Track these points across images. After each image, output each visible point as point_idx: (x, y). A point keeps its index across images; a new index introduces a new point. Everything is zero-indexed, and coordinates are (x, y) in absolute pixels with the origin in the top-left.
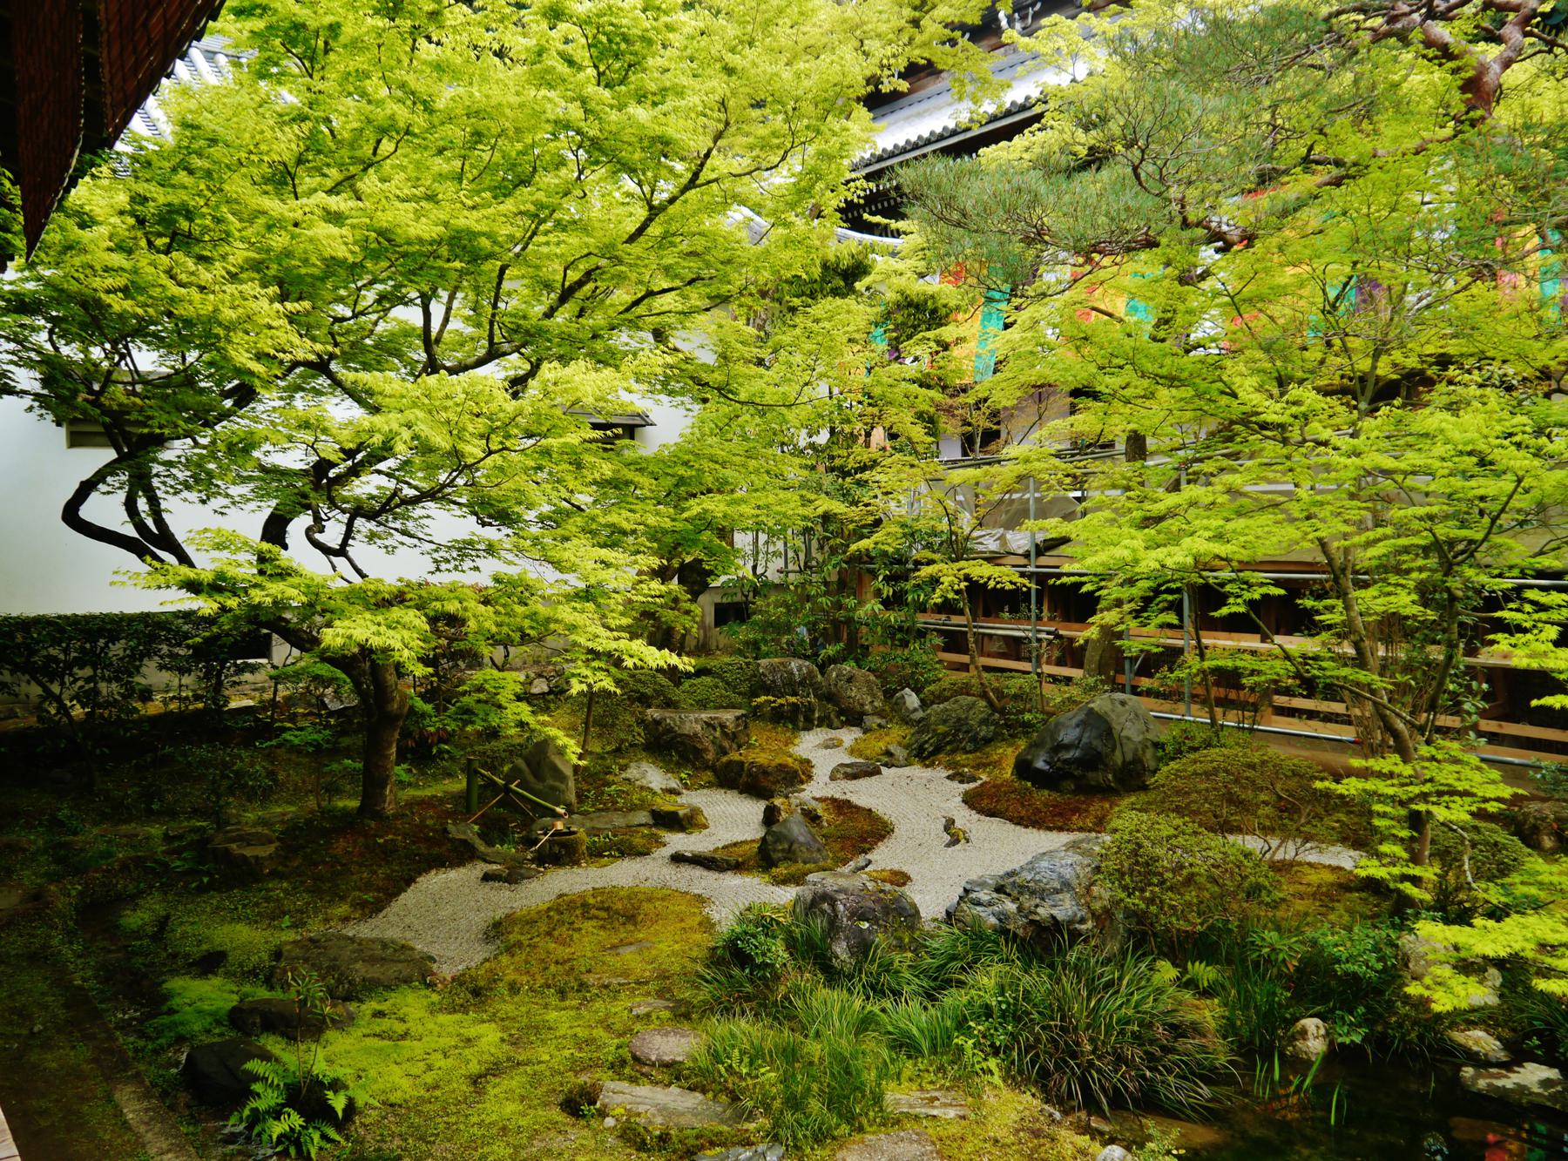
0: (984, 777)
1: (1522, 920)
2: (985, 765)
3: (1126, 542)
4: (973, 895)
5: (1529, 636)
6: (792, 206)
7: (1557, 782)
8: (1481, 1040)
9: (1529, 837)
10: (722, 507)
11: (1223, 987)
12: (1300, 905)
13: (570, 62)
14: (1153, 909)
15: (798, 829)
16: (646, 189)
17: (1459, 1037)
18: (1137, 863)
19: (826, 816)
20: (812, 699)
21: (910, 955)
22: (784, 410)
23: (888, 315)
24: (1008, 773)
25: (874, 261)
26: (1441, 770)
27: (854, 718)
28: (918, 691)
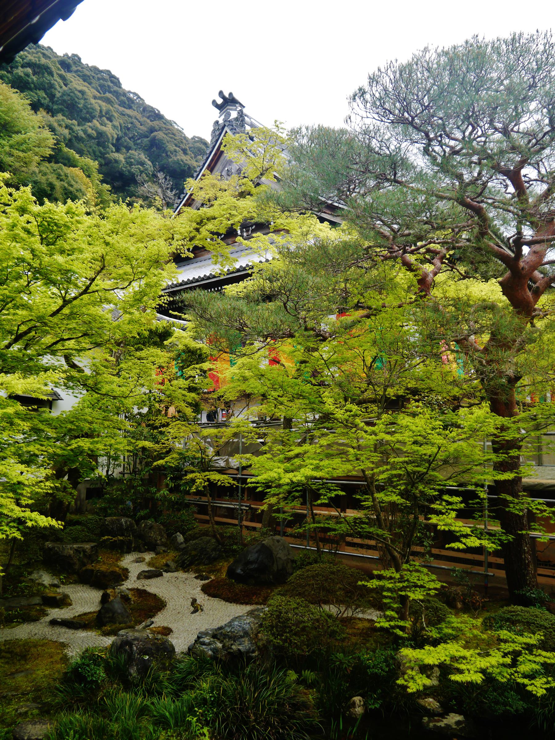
0: (213, 577)
1: (445, 646)
2: (214, 571)
3: (276, 470)
4: (202, 640)
5: (444, 516)
6: (132, 306)
7: (462, 578)
8: (431, 703)
9: (451, 604)
10: (88, 445)
11: (318, 682)
12: (354, 639)
13: (28, 232)
14: (286, 645)
15: (118, 606)
16: (63, 292)
17: (422, 702)
18: (279, 622)
19: (133, 598)
20: (131, 538)
21: (168, 672)
22: (123, 399)
23: (179, 355)
24: (224, 576)
25: (174, 330)
26: (411, 575)
27: (151, 547)
28: (183, 534)
